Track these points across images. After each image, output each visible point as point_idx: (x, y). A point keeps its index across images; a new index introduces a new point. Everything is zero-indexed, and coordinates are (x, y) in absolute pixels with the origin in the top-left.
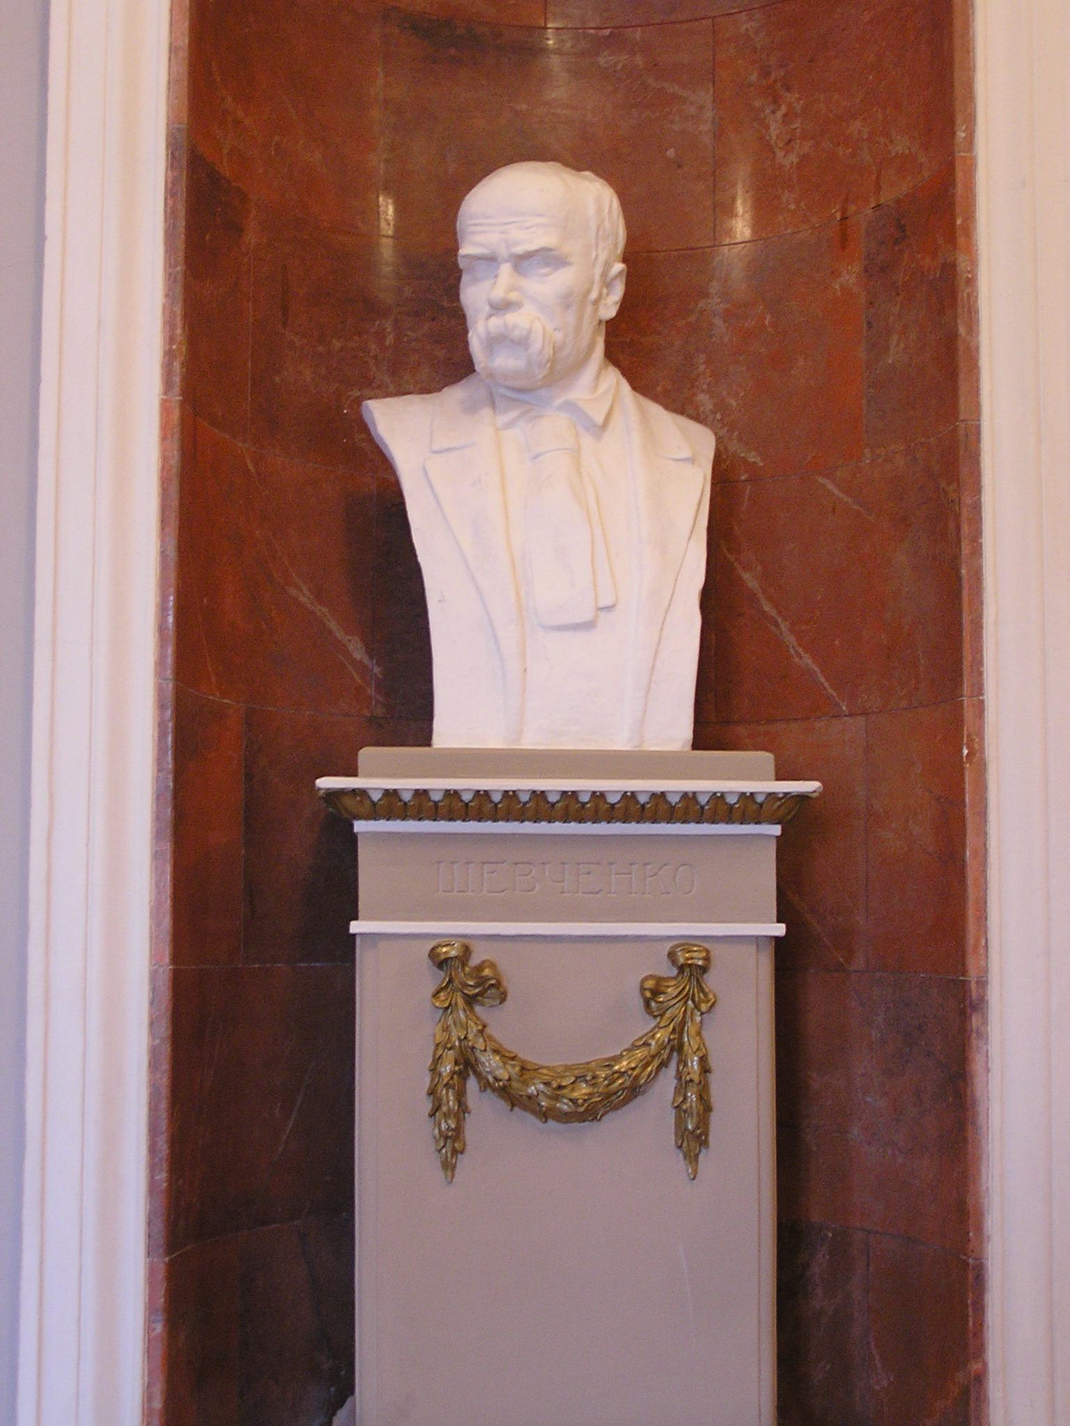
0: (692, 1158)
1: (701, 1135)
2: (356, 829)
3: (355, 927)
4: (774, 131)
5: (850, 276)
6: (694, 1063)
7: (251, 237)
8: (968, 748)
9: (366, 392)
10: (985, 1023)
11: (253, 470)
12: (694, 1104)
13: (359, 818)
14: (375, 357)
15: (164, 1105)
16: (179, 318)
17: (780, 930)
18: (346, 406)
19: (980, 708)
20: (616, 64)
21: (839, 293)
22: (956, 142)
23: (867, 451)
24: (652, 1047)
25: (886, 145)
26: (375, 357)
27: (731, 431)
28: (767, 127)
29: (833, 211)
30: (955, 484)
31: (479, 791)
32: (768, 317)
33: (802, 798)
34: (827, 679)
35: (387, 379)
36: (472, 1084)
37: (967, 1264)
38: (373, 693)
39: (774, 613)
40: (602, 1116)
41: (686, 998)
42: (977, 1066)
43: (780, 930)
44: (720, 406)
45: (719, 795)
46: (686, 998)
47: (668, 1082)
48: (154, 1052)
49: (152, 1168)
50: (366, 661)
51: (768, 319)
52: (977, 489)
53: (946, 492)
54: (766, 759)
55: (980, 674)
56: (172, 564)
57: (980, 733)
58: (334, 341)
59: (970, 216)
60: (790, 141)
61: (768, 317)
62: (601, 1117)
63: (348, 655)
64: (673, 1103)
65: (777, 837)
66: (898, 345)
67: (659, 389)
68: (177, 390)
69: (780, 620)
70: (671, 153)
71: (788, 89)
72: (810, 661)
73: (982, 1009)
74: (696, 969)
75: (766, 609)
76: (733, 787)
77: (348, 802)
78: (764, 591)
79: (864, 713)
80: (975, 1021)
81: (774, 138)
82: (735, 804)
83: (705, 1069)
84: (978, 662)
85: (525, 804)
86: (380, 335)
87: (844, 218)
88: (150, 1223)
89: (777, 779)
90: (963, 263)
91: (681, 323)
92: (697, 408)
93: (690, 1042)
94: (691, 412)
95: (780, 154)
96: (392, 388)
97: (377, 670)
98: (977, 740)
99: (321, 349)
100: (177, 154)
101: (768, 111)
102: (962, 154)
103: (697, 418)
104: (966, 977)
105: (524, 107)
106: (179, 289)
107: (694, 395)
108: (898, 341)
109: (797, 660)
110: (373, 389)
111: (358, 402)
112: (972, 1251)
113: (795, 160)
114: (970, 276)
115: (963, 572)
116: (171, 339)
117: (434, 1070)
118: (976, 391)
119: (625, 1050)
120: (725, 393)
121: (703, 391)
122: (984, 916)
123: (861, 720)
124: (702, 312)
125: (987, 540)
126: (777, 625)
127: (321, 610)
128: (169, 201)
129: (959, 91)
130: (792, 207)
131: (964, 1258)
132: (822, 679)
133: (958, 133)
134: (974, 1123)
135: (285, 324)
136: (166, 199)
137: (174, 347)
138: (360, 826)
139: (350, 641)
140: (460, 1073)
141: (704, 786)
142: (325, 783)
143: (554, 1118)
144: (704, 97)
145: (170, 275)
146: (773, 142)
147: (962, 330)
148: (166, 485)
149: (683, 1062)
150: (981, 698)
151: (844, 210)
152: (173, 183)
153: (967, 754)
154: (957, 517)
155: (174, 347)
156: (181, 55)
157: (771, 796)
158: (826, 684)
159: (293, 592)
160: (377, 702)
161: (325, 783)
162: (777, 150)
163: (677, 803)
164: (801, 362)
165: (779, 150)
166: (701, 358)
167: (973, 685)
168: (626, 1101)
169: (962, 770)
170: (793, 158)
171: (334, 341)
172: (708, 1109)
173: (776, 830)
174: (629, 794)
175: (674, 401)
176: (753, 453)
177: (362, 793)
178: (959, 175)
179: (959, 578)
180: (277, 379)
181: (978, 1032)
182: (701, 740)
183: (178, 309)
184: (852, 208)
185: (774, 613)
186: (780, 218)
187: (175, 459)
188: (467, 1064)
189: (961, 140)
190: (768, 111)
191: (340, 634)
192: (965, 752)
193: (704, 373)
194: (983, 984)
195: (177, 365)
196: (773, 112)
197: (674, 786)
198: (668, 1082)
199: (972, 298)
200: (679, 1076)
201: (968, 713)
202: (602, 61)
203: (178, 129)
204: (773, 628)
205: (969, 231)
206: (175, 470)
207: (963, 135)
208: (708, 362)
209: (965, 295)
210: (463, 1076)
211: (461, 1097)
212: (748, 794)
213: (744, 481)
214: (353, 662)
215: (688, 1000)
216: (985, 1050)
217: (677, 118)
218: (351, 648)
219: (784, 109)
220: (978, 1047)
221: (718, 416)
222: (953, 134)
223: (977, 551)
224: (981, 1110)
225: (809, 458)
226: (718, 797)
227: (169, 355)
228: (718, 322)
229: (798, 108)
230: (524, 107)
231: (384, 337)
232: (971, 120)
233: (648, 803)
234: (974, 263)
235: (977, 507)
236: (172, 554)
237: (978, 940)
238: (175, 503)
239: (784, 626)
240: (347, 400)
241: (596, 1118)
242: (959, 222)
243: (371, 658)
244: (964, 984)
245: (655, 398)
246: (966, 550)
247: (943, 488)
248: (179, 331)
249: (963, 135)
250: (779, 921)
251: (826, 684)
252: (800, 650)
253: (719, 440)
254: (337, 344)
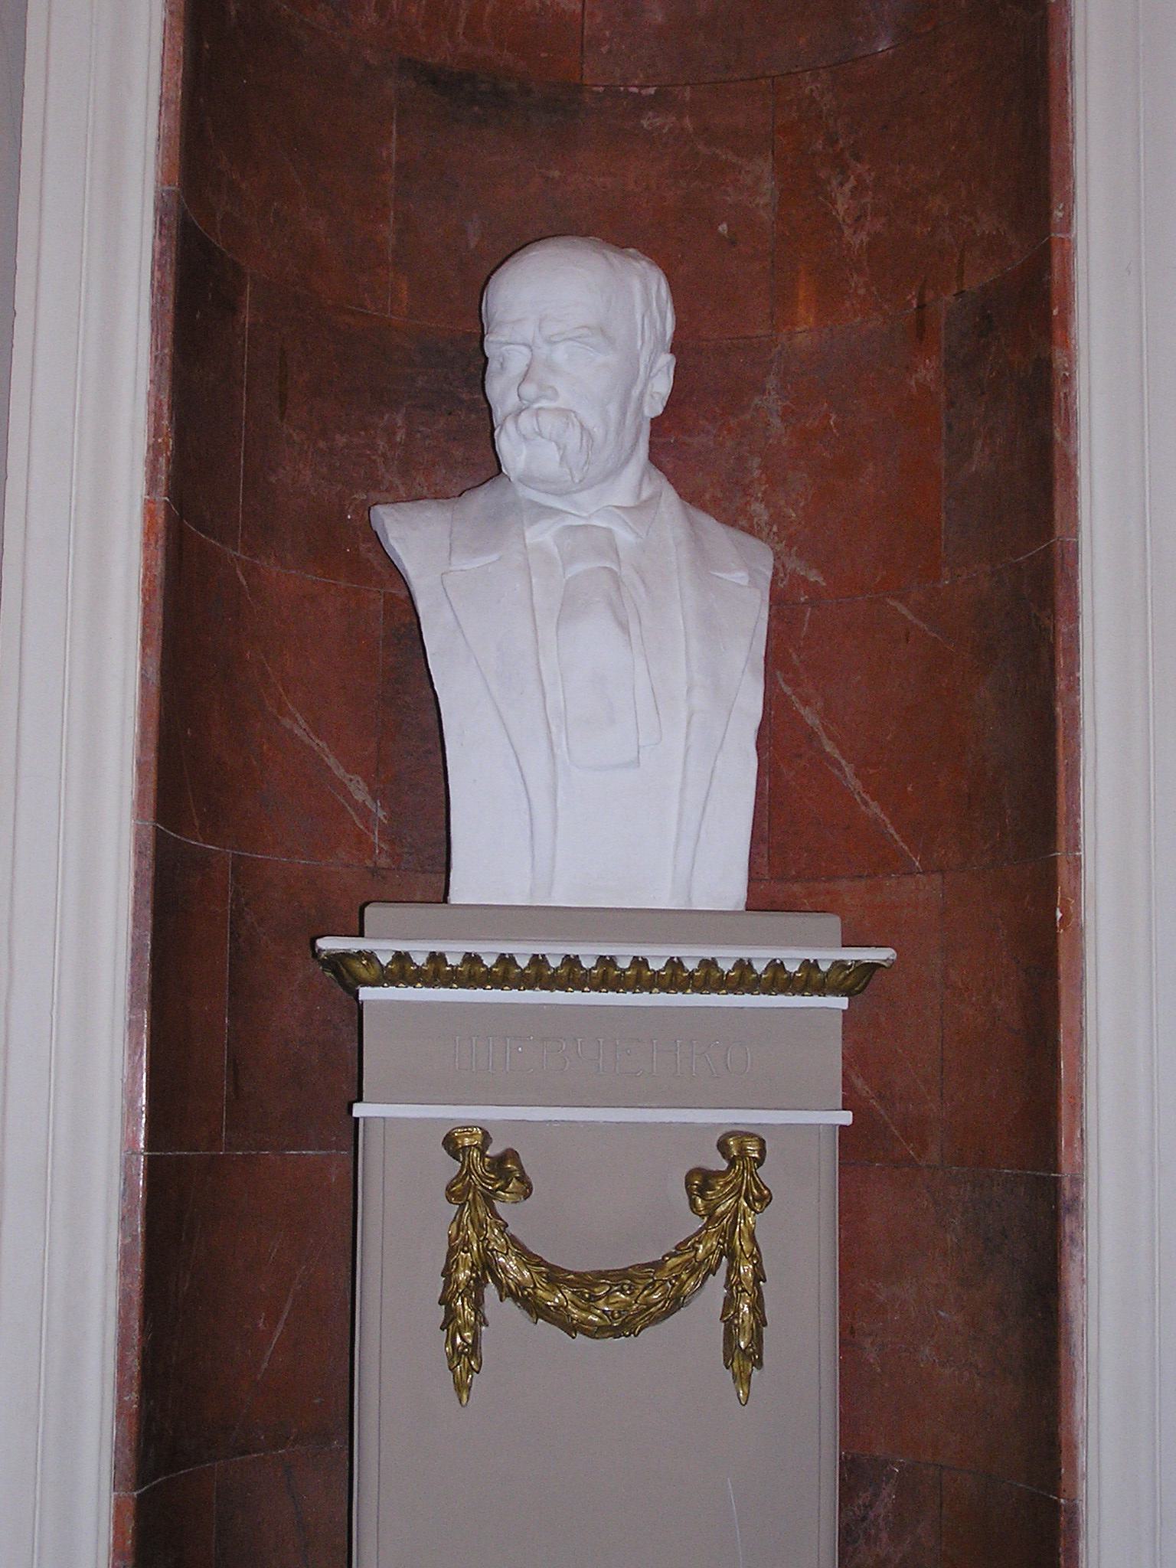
0: (742, 1379)
1: (753, 1354)
2: (361, 997)
3: (359, 1110)
4: (841, 206)
5: (927, 372)
6: (746, 1269)
7: (246, 317)
8: (1061, 912)
9: (374, 495)
10: (1080, 1227)
11: (245, 583)
12: (746, 1319)
13: (366, 984)
14: (384, 455)
15: (135, 1314)
16: (165, 408)
17: (846, 1118)
18: (350, 510)
19: (1076, 866)
20: (662, 127)
21: (915, 391)
22: (1052, 222)
23: (946, 570)
24: (700, 1251)
25: (970, 224)
26: (384, 455)
27: (789, 546)
28: (834, 203)
29: (909, 298)
30: (1049, 610)
31: (504, 954)
32: (834, 416)
33: (873, 967)
34: (898, 831)
35: (397, 481)
36: (491, 1291)
37: (1057, 1504)
38: (376, 841)
39: (837, 755)
40: (639, 1331)
41: (738, 1195)
42: (1071, 1273)
43: (846, 1118)
44: (778, 517)
45: (778, 962)
46: (738, 1195)
47: (716, 1287)
48: (125, 1254)
49: (121, 1388)
50: (369, 803)
51: (833, 418)
52: (1074, 616)
53: (1038, 619)
54: (832, 923)
55: (1077, 827)
56: (154, 690)
57: (1076, 895)
58: (338, 436)
59: (1067, 308)
60: (859, 217)
61: (834, 416)
62: (639, 1331)
63: (348, 795)
64: (722, 1316)
65: (843, 1011)
66: (982, 450)
67: (707, 496)
68: (162, 489)
69: (843, 762)
70: (723, 228)
71: (858, 158)
72: (878, 811)
73: (1077, 1210)
74: (750, 1160)
75: (828, 749)
76: (792, 959)
77: (359, 968)
78: (825, 728)
79: (941, 871)
80: (1068, 1225)
81: (842, 213)
82: (796, 972)
83: (759, 1276)
84: (1074, 813)
85: (556, 970)
86: (390, 432)
87: (921, 306)
88: (117, 1451)
89: (843, 946)
90: (1059, 359)
91: (733, 422)
92: (751, 518)
93: (742, 1244)
94: (744, 523)
95: (847, 232)
96: (402, 491)
97: (381, 814)
98: (1073, 901)
99: (322, 444)
100: (166, 220)
101: (834, 183)
102: (1059, 235)
103: (751, 531)
104: (1059, 1173)
105: (557, 174)
106: (166, 376)
107: (748, 503)
108: (983, 446)
109: (863, 808)
110: (380, 491)
111: (367, 507)
112: (1064, 1491)
113: (866, 239)
114: (1067, 374)
115: (1058, 710)
116: (156, 432)
117: (448, 1273)
118: (1073, 504)
119: (667, 1255)
120: (782, 503)
121: (757, 499)
122: (1074, 585)
123: (937, 878)
124: (757, 409)
125: (1085, 673)
126: (841, 769)
127: (319, 744)
128: (156, 273)
129: (1056, 165)
130: (862, 292)
131: (1056, 1498)
132: (892, 831)
133: (1055, 212)
134: (1067, 1343)
135: (282, 419)
136: (152, 273)
137: (160, 440)
138: (365, 993)
139: (351, 780)
140: (476, 1280)
141: (760, 958)
142: (326, 944)
143: (585, 1332)
144: (763, 166)
145: (156, 357)
146: (840, 218)
147: (1058, 435)
148: (147, 599)
149: (732, 1269)
150: (1077, 854)
151: (921, 296)
152: (162, 254)
153: (1062, 917)
154: (1052, 647)
155: (160, 440)
156: (173, 107)
157: (839, 965)
158: (896, 837)
159: (287, 722)
160: (381, 849)
161: (326, 944)
162: (845, 228)
163: (730, 971)
164: (871, 468)
165: (846, 227)
166: (756, 461)
167: (1067, 840)
168: (668, 1313)
169: (1056, 935)
170: (864, 237)
171: (338, 436)
172: (761, 1322)
173: (842, 1003)
174: (675, 959)
175: (725, 510)
176: (815, 571)
177: (370, 956)
178: (1056, 260)
179: (1053, 718)
180: (273, 479)
181: (1072, 1240)
182: (760, 899)
183: (165, 398)
184: (930, 295)
185: (837, 755)
186: (848, 304)
187: (159, 568)
188: (487, 1266)
189: (1058, 221)
190: (834, 183)
191: (340, 772)
192: (1059, 915)
193: (759, 479)
194: (1077, 1181)
195: (162, 461)
196: (841, 184)
197: (726, 958)
198: (716, 1287)
199: (1069, 399)
200: (728, 1284)
201: (1063, 871)
202: (645, 123)
203: (169, 193)
204: (836, 772)
205: (1065, 324)
206: (158, 582)
207: (1060, 214)
208: (764, 468)
209: (1062, 395)
210: (479, 1284)
211: (478, 1305)
212: (812, 961)
213: (803, 603)
214: (355, 805)
215: (739, 1198)
216: (1080, 1258)
217: (730, 189)
218: (352, 787)
219: (852, 182)
220: (1071, 1255)
221: (775, 529)
222: (1049, 214)
223: (1074, 687)
224: (1076, 1327)
225: (878, 579)
226: (777, 964)
227: (154, 449)
228: (776, 422)
229: (869, 180)
230: (557, 174)
231: (395, 433)
232: (1069, 198)
233: (697, 971)
234: (1071, 359)
235: (1074, 636)
236: (154, 678)
237: (1072, 1132)
238: (158, 619)
239: (848, 770)
240: (351, 504)
241: (634, 1333)
242: (1055, 312)
243: (374, 800)
244: (1057, 1181)
245: (703, 508)
246: (1061, 685)
247: (1035, 615)
248: (165, 422)
249: (1060, 214)
250: (357, 1119)
251: (896, 837)
252: (867, 798)
253: (777, 556)
254: (341, 440)
